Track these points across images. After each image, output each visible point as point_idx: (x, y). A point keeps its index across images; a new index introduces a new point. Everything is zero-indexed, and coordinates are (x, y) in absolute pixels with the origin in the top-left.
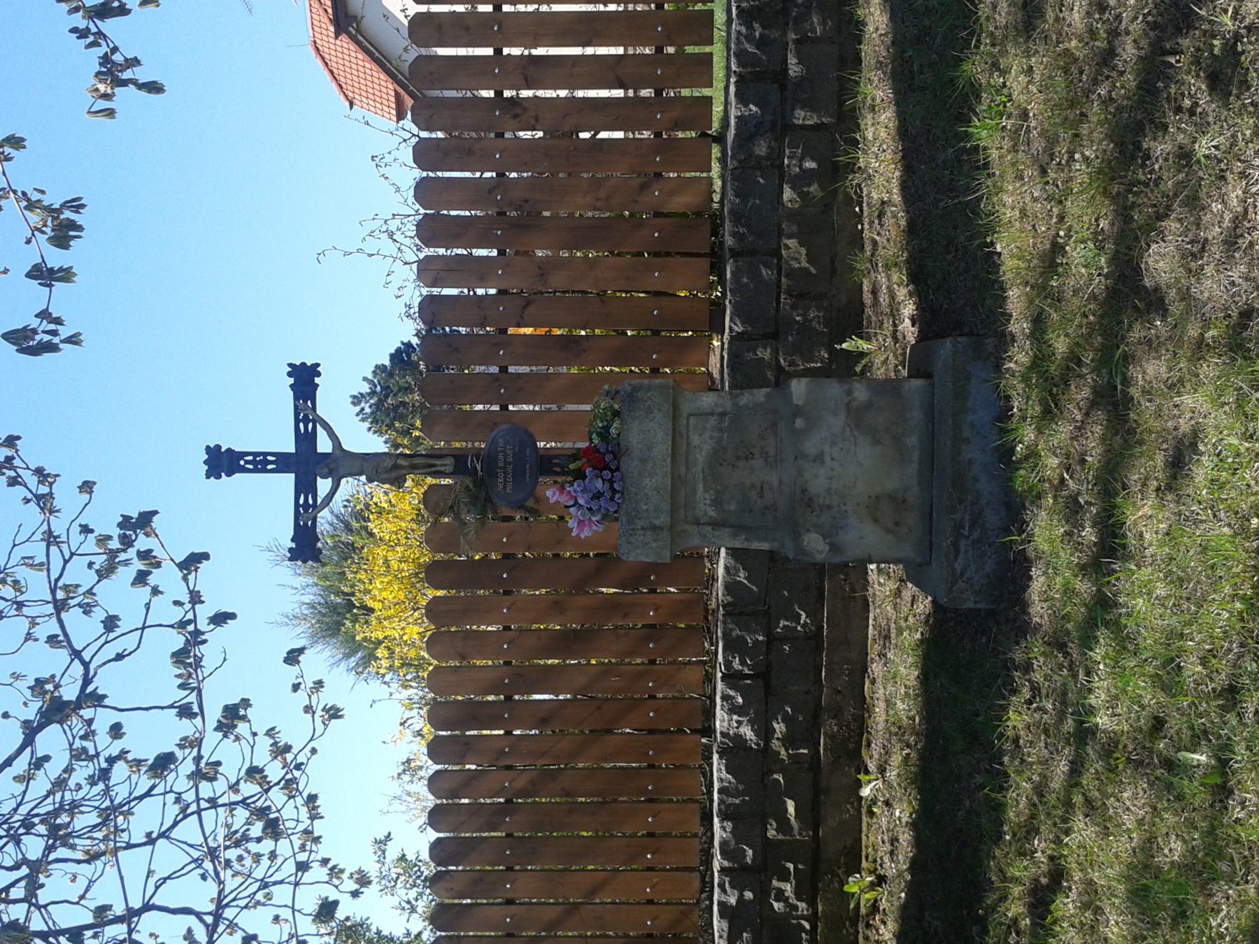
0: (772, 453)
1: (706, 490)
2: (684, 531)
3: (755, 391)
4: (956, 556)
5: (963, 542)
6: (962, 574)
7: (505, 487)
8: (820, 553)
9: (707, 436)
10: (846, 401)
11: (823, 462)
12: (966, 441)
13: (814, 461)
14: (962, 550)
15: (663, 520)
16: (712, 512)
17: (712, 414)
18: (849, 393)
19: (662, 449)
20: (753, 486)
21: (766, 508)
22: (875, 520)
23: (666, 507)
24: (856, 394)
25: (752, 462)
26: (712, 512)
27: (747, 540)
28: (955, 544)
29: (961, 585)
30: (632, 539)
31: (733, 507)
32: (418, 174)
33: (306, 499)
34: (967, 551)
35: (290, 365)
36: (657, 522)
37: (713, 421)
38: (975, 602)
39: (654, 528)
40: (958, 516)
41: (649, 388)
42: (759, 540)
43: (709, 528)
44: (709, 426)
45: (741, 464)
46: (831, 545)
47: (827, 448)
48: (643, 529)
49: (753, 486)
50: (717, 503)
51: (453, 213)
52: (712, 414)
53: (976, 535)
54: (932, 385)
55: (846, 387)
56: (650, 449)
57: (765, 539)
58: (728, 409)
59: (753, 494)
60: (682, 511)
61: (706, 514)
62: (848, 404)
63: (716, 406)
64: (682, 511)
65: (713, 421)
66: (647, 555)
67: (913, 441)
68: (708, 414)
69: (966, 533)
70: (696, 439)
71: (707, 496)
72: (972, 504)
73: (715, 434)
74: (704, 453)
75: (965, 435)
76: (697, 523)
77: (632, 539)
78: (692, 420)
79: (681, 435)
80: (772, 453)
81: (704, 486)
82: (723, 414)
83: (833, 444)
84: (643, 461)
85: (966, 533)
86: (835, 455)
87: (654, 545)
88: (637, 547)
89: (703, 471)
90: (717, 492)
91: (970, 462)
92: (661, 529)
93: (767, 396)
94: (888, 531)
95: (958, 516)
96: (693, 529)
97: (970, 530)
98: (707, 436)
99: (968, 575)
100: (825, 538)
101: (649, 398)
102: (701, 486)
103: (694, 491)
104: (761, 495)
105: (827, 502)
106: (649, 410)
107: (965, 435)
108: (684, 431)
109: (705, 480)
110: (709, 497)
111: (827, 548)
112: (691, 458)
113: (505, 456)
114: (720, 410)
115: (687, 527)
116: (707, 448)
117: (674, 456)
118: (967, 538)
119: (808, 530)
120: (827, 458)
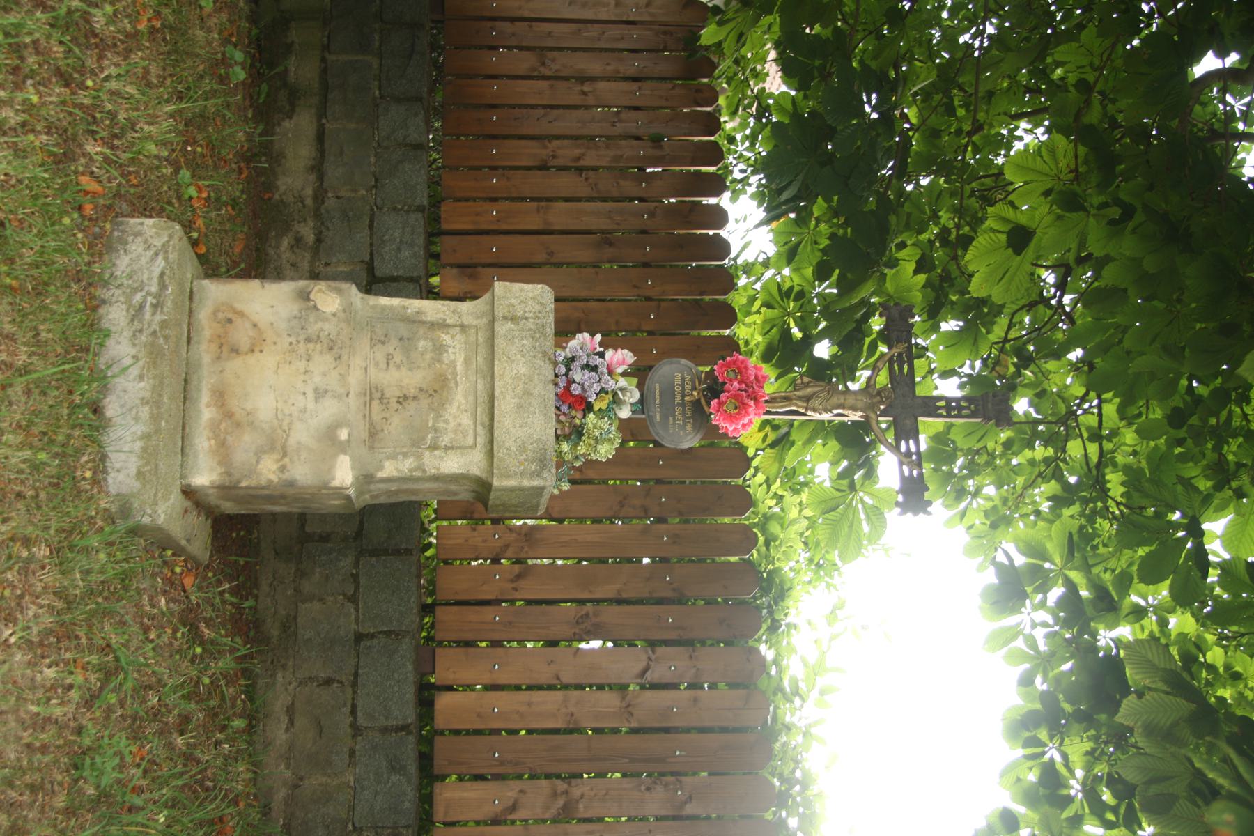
0: (375, 403)
1: (453, 364)
2: (478, 318)
3: (395, 474)
4: (162, 274)
5: (154, 289)
6: (156, 254)
7: (683, 379)
8: (320, 291)
9: (452, 424)
10: (287, 460)
11: (316, 390)
12: (144, 402)
13: (326, 392)
14: (155, 281)
15: (502, 328)
16: (446, 338)
17: (447, 448)
18: (283, 469)
19: (505, 405)
20: (398, 367)
21: (383, 343)
22: (255, 325)
23: (500, 343)
24: (274, 467)
25: (398, 394)
26: (446, 338)
27: (405, 308)
28: (163, 287)
29: (158, 243)
30: (538, 307)
31: (421, 344)
32: (723, 233)
33: (901, 369)
34: (150, 279)
35: (929, 514)
36: (510, 325)
37: (445, 440)
38: (142, 224)
39: (513, 319)
40: (158, 317)
41: (522, 474)
42: (391, 308)
43: (448, 321)
44: (451, 435)
45: (413, 392)
46: (308, 299)
47: (311, 405)
48: (526, 319)
49: (398, 367)
50: (440, 349)
51: (696, 139)
52: (447, 448)
53: (138, 297)
54: (182, 477)
55: (286, 476)
56: (520, 406)
57: (383, 308)
58: (427, 453)
59: (398, 357)
60: (481, 340)
61: (453, 337)
62: (285, 455)
63: (441, 458)
64: (481, 340)
65: (445, 440)
66: (521, 290)
67: (206, 413)
68: (452, 448)
69: (149, 299)
70: (466, 420)
71: (452, 357)
72: (141, 331)
73: (441, 425)
74: (456, 404)
75: (147, 408)
76: (463, 327)
77: (538, 307)
78: (470, 441)
79: (482, 424)
80: (375, 403)
81: (455, 367)
82: (434, 447)
83: (304, 411)
84: (527, 393)
85: (149, 299)
86: (301, 397)
87: (513, 301)
88: (533, 298)
89: (457, 384)
90: (439, 361)
91: (141, 377)
92: (505, 318)
93: (381, 468)
94: (241, 314)
95: (158, 317)
96: (467, 320)
97: (145, 301)
98: (452, 424)
99: (150, 253)
100: (315, 307)
101: (521, 464)
102: (460, 367)
103: (467, 361)
104: (389, 358)
105: (311, 346)
106: (522, 449)
107: (147, 408)
108: (479, 428)
109: (455, 374)
110: (448, 357)
111: (312, 296)
112: (471, 399)
113: (684, 413)
114: (436, 453)
115: (475, 323)
116: (452, 409)
117: (492, 398)
118: (149, 293)
119: (334, 315)
120: (310, 395)
